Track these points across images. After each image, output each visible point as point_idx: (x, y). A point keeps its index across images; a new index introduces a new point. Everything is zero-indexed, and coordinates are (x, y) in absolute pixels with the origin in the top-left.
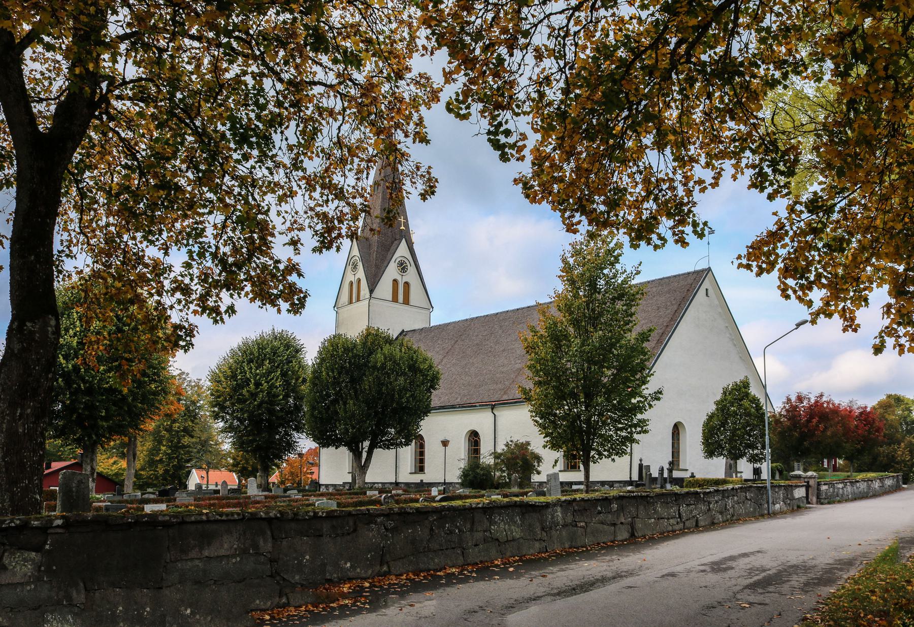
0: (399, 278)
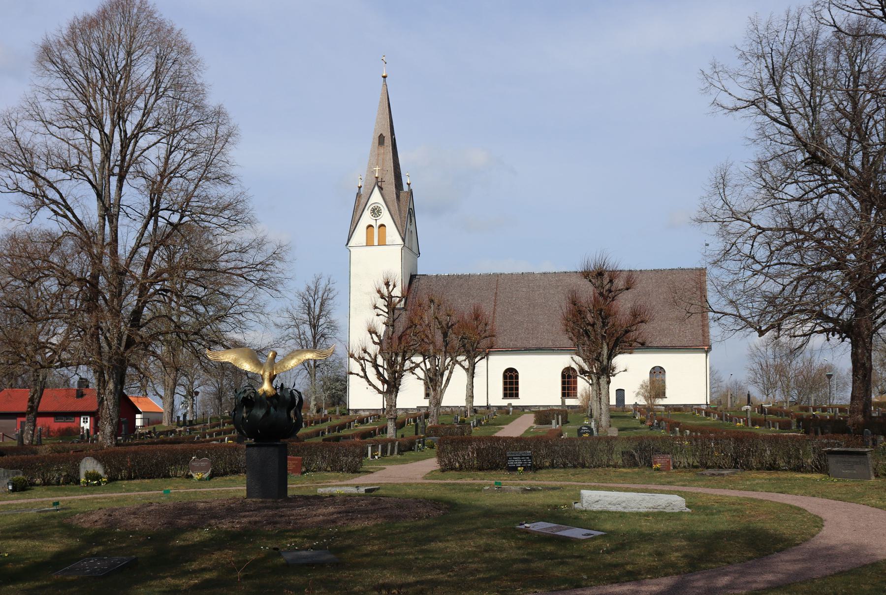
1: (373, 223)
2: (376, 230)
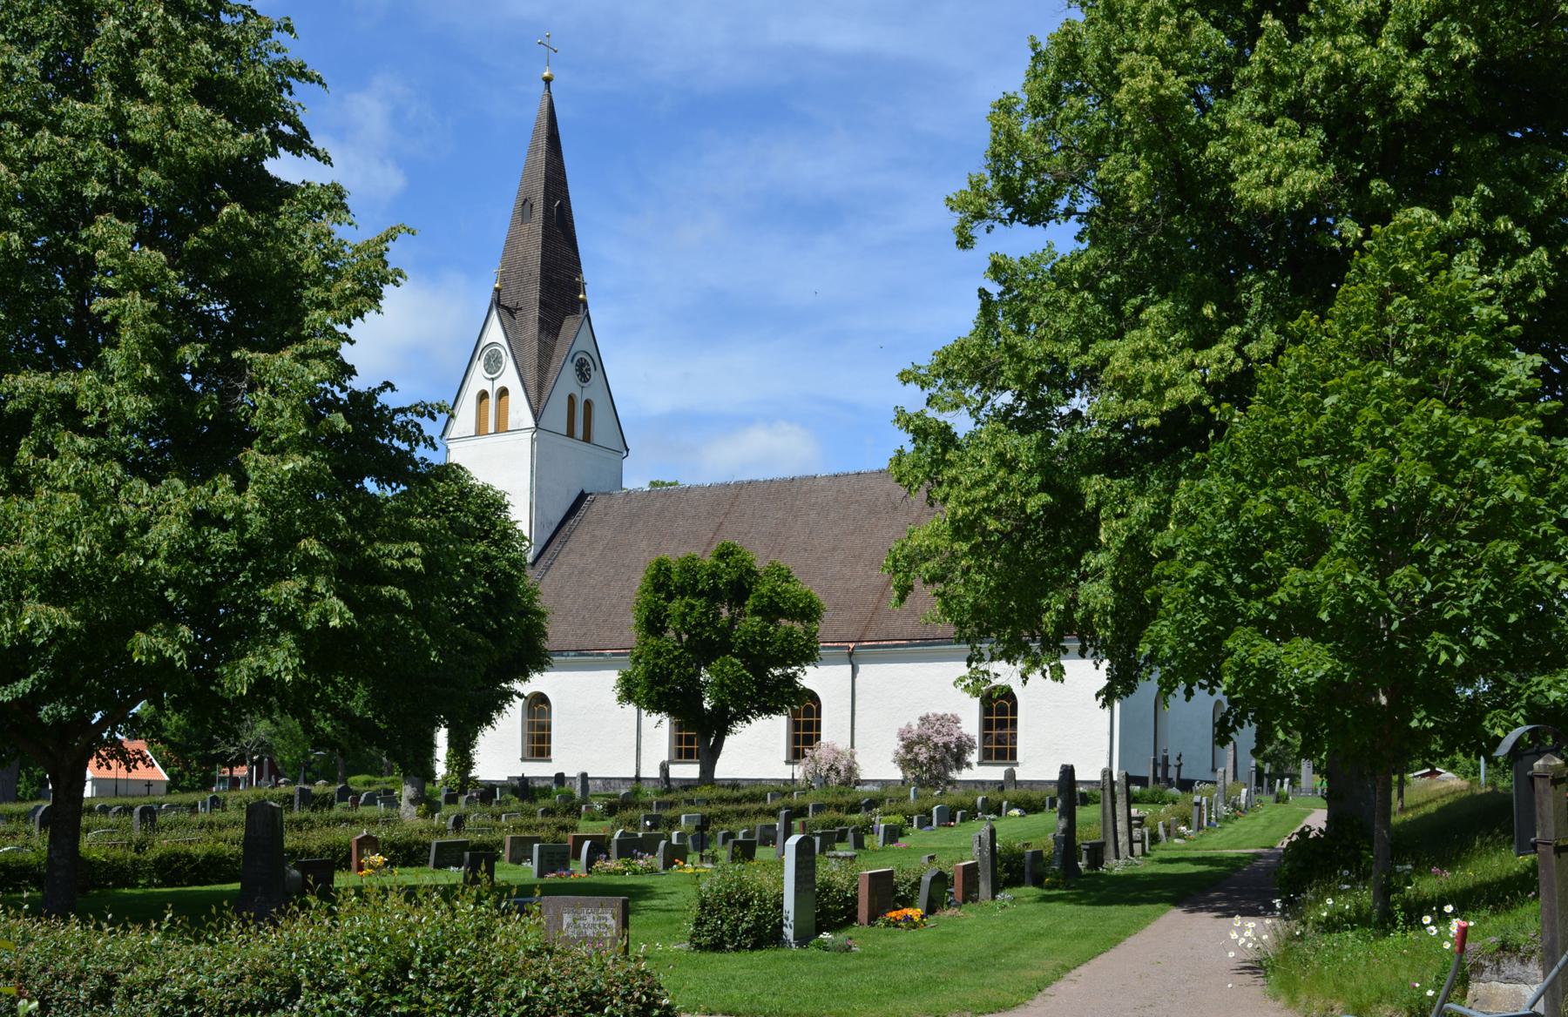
0: (577, 393)
1: (487, 386)
2: (492, 401)
